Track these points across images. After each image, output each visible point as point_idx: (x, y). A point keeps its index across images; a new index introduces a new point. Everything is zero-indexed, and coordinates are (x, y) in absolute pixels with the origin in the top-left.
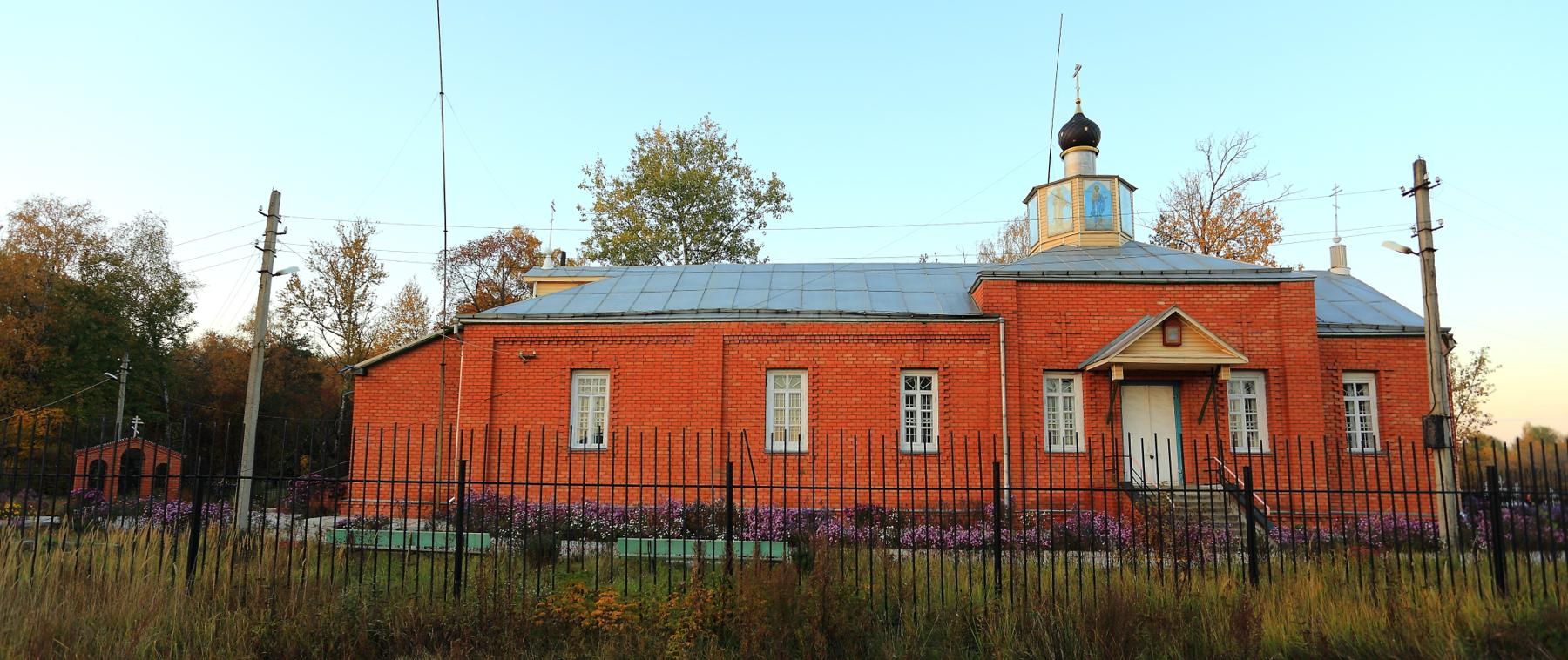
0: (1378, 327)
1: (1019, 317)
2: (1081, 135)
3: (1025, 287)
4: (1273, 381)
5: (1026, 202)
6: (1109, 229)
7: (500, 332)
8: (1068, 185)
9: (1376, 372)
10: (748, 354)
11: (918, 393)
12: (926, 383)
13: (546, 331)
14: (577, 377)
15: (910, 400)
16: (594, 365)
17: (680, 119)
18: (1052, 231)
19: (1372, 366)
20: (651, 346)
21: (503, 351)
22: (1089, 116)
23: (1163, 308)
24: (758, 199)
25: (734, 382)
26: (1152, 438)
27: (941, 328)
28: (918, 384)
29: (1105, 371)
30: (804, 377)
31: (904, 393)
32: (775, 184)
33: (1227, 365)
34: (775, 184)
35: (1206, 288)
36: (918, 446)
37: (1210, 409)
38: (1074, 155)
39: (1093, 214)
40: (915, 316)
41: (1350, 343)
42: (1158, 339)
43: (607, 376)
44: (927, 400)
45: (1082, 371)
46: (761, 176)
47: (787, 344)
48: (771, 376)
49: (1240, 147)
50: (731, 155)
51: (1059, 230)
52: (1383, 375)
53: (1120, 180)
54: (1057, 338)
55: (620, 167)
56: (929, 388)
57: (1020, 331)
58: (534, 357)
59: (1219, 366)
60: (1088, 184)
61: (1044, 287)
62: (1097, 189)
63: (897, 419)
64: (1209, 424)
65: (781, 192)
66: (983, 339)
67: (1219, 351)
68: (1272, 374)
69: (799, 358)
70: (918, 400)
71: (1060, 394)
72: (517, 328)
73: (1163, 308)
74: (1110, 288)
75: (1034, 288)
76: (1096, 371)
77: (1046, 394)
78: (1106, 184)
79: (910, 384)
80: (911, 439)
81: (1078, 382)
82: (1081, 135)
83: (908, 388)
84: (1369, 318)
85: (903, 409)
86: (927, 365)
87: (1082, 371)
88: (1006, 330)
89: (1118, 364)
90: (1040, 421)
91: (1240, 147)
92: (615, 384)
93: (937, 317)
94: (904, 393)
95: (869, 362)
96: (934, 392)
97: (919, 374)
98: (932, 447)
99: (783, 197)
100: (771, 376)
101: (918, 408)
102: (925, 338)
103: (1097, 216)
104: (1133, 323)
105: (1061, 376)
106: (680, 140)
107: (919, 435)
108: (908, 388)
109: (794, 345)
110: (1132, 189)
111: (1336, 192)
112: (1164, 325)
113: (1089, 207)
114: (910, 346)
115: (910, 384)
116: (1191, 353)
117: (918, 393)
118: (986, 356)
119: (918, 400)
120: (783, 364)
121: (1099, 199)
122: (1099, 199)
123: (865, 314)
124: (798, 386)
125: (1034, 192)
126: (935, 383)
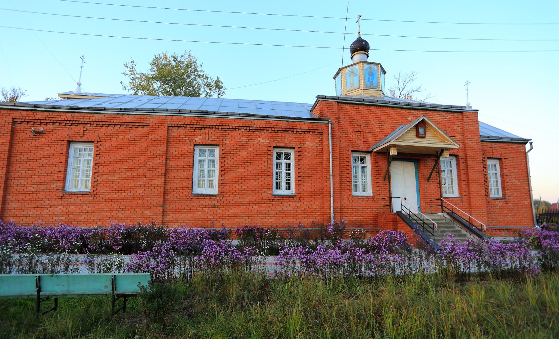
0: (501, 138)
1: (339, 122)
2: (361, 47)
3: (342, 106)
4: (461, 161)
5: (335, 78)
6: (377, 88)
7: (18, 115)
8: (357, 67)
9: (500, 159)
10: (184, 136)
11: (283, 161)
12: (288, 156)
13: (51, 116)
14: (73, 147)
15: (279, 165)
16: (84, 139)
17: (175, 49)
18: (349, 89)
19: (498, 156)
20: (122, 128)
21: (18, 127)
22: (363, 38)
23: (410, 121)
24: (209, 86)
25: (174, 152)
26: (405, 191)
27: (297, 125)
28: (283, 156)
29: (385, 153)
30: (217, 150)
31: (275, 161)
32: (218, 81)
33: (447, 149)
34: (218, 81)
35: (430, 112)
36: (283, 192)
37: (434, 174)
38: (358, 57)
39: (369, 80)
40: (282, 117)
41: (490, 144)
42: (414, 134)
43: (92, 146)
44: (288, 166)
45: (370, 152)
46: (213, 77)
47: (207, 130)
48: (197, 149)
49: (410, 79)
50: (199, 69)
51: (352, 88)
52: (504, 160)
53: (381, 66)
54: (358, 134)
55: (145, 68)
56: (289, 159)
57: (339, 130)
58: (40, 133)
59: (443, 150)
60: (367, 66)
61: (352, 106)
62: (371, 68)
63: (271, 176)
64: (434, 181)
65: (220, 85)
66: (320, 132)
67: (443, 140)
68: (461, 157)
69: (214, 139)
70: (283, 166)
71: (359, 164)
72: (30, 113)
73: (410, 121)
74: (385, 109)
75: (347, 106)
76: (378, 153)
77: (353, 165)
78: (375, 67)
79: (279, 156)
80: (279, 188)
81: (368, 158)
82: (361, 47)
83: (277, 158)
84: (493, 134)
85: (275, 170)
86: (288, 145)
87: (370, 152)
88: (332, 128)
89: (394, 146)
90: (350, 178)
91: (410, 79)
92: (98, 150)
93: (294, 118)
94: (275, 161)
95: (256, 142)
96: (292, 161)
97: (284, 151)
98: (292, 192)
99: (222, 87)
100: (197, 149)
101: (283, 170)
102: (287, 130)
103: (371, 81)
104: (396, 129)
105: (360, 155)
106: (175, 59)
107: (283, 185)
108: (277, 158)
109: (211, 131)
110: (385, 73)
111: (467, 83)
112: (417, 127)
113: (367, 77)
114: (279, 134)
115: (279, 156)
116: (430, 142)
117: (283, 161)
118: (322, 142)
119: (283, 166)
120: (204, 142)
121: (371, 74)
122: (371, 74)
123: (254, 115)
124: (214, 156)
125: (340, 70)
126: (293, 157)
